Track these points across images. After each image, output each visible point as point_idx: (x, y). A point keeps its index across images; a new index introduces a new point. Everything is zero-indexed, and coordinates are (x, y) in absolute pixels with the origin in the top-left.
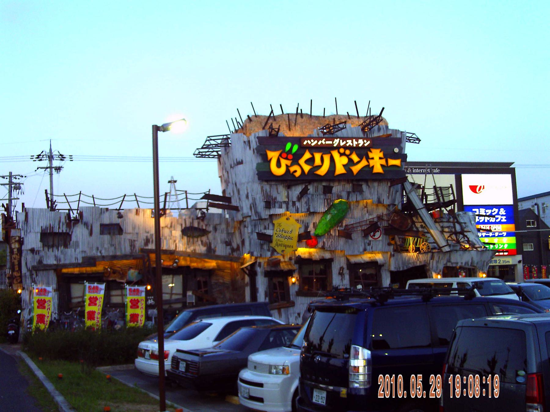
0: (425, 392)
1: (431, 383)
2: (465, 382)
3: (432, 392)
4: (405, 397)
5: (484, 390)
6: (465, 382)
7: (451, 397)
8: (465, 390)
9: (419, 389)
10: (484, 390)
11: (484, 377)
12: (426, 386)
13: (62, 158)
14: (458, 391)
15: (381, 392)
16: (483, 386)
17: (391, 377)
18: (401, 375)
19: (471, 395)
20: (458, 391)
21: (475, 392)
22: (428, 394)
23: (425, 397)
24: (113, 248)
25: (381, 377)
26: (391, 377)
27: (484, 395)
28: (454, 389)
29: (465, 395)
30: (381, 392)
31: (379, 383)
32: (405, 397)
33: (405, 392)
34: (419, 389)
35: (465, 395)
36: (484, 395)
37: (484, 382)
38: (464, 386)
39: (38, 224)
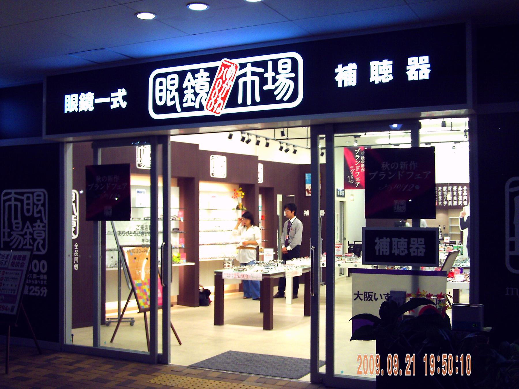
0: (401, 370)
1: (406, 362)
2: (439, 361)
3: (408, 370)
4: (382, 375)
5: (457, 368)
6: (439, 361)
7: (426, 375)
8: (439, 368)
9: (444, 367)
10: (457, 368)
11: (457, 356)
12: (402, 365)
13: (295, 152)
14: (432, 369)
15: (408, 370)
16: (457, 365)
17: (411, 356)
18: (396, 354)
19: (390, 373)
20: (432, 369)
21: (447, 370)
22: (403, 372)
23: (401, 375)
24: (464, 271)
25: (408, 356)
26: (411, 356)
27: (457, 373)
28: (429, 368)
29: (439, 373)
30: (408, 370)
31: (406, 362)
32: (382, 375)
33: (382, 370)
34: (444, 367)
35: (439, 373)
36: (457, 373)
37: (457, 361)
38: (438, 365)
39: (343, 239)
